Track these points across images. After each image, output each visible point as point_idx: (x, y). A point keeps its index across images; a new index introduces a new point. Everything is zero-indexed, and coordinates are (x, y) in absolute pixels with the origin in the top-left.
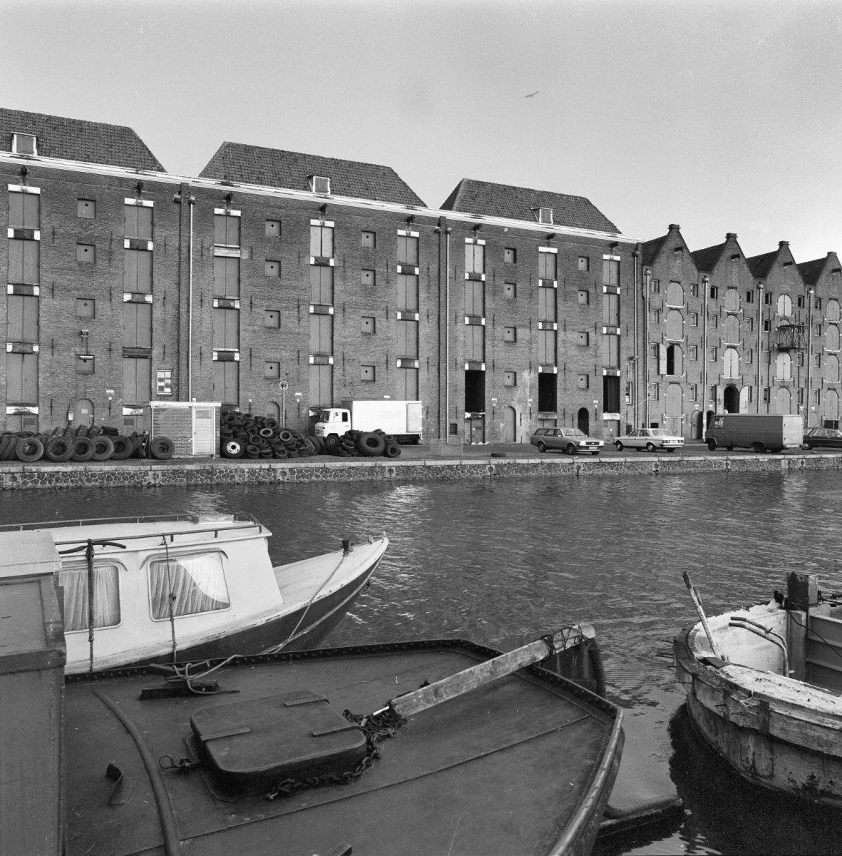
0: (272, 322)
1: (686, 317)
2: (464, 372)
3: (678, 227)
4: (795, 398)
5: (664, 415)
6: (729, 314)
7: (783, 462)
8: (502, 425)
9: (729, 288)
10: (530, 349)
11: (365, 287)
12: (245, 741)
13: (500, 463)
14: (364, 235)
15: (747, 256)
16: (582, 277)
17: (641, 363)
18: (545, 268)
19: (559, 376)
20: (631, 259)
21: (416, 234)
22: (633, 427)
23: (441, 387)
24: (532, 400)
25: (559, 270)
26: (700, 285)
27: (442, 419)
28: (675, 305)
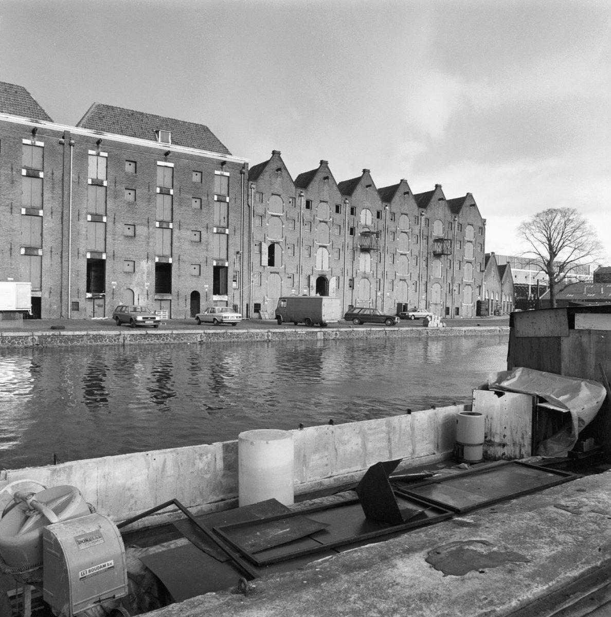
0: (130, 233)
1: (285, 222)
2: (86, 260)
3: (326, 163)
4: (374, 286)
5: (266, 297)
6: (320, 221)
7: (319, 334)
9: (321, 201)
10: (148, 243)
11: (129, 204)
12: (557, 437)
13: (44, 334)
14: (194, 174)
15: (414, 193)
16: (196, 187)
17: (246, 256)
18: (163, 178)
19: (107, 260)
20: (240, 175)
21: (39, 143)
22: (239, 306)
23: (64, 272)
24: (149, 284)
25: (175, 181)
26: (297, 199)
27: (64, 298)
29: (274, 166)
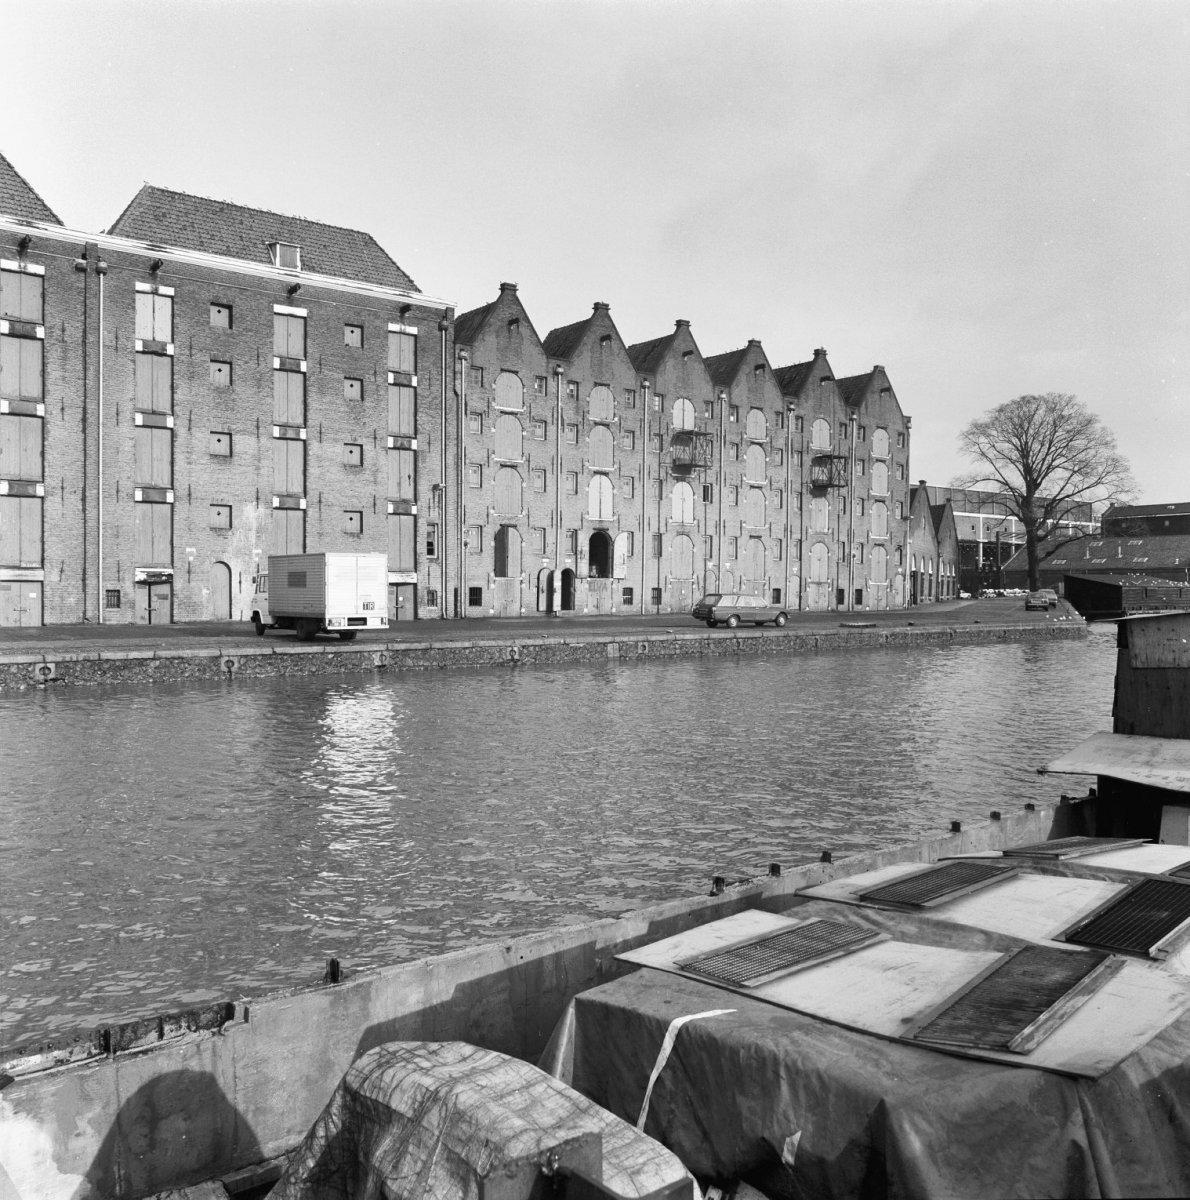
3: (606, 307)
4: (700, 550)
6: (596, 424)
7: (610, 647)
8: (205, 591)
10: (258, 468)
20: (438, 333)
22: (439, 594)
24: (260, 551)
28: (509, 406)
29: (505, 314)
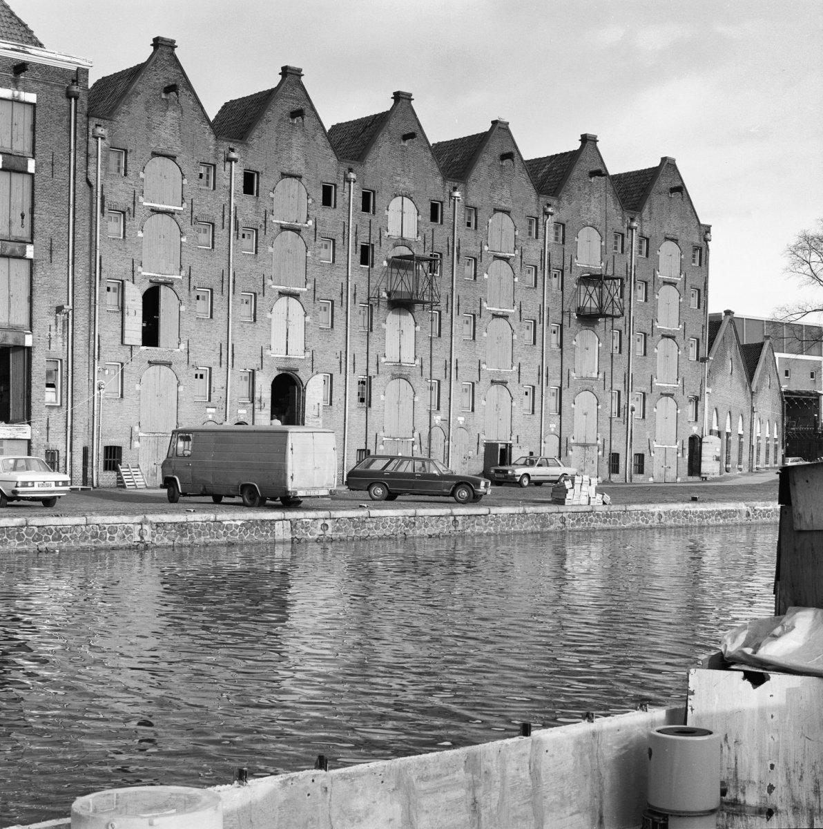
29: (159, 78)
